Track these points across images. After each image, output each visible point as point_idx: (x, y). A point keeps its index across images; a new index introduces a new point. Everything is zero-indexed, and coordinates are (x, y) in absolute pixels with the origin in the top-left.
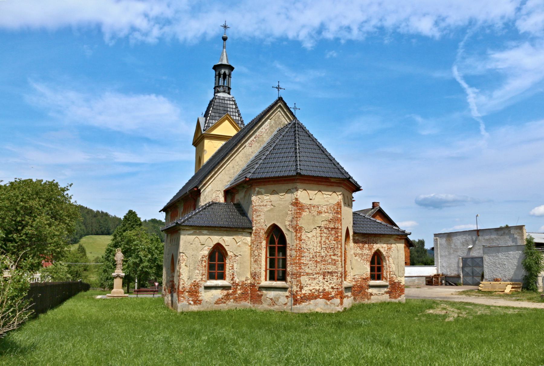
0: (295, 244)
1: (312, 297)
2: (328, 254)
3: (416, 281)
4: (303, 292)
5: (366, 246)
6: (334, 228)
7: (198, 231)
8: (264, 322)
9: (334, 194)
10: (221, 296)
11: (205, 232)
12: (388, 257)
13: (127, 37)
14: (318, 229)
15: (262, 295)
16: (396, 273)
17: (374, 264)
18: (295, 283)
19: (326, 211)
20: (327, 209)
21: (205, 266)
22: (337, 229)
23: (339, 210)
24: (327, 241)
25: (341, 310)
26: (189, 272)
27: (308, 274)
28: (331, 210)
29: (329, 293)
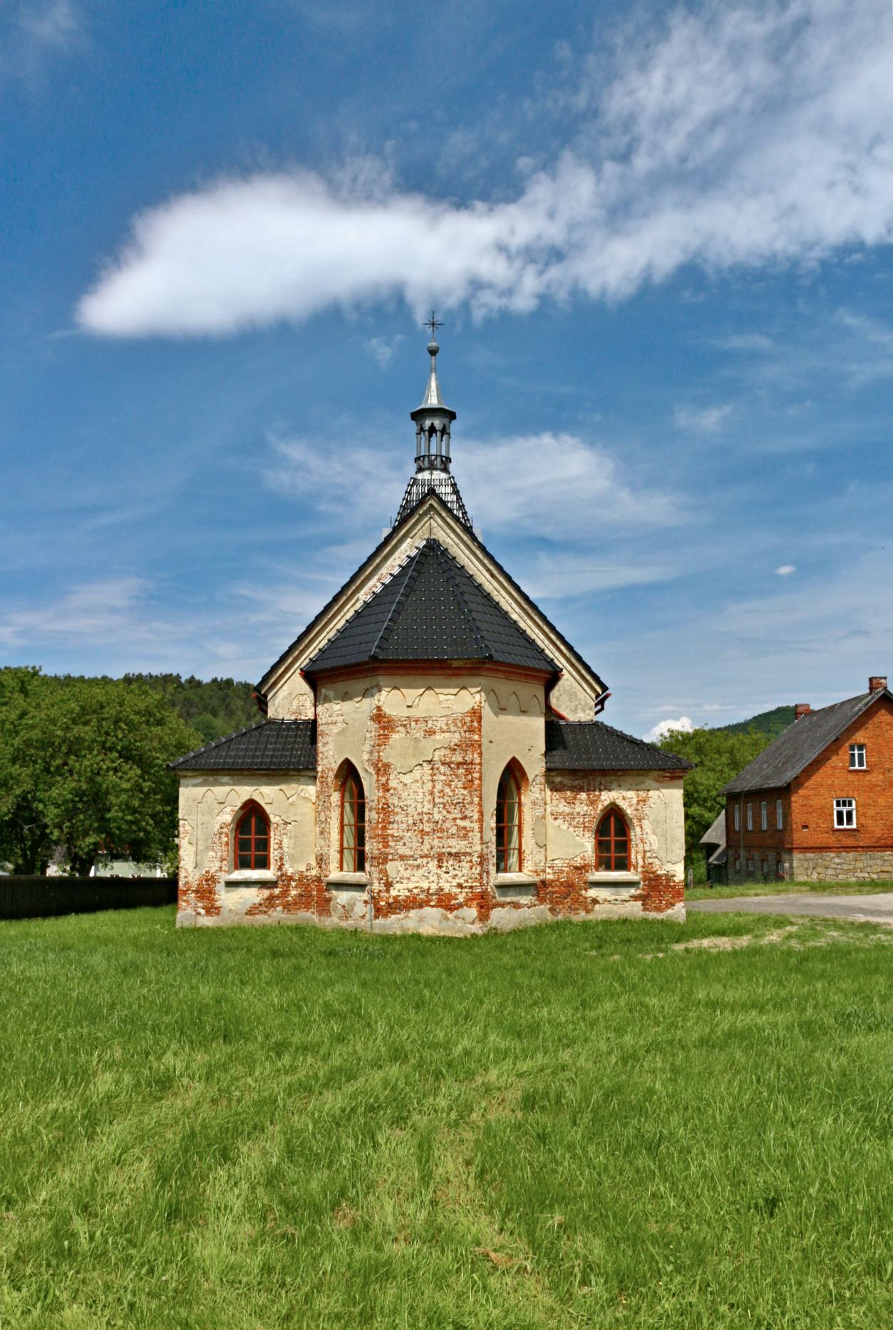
1: (397, 906)
2: (448, 816)
4: (393, 893)
5: (583, 795)
6: (465, 763)
7: (211, 779)
8: (351, 952)
9: (464, 692)
10: (257, 900)
11: (225, 779)
12: (640, 820)
13: (465, 306)
15: (330, 899)
16: (662, 855)
18: (375, 875)
19: (445, 728)
20: (447, 724)
21: (227, 844)
22: (472, 763)
23: (476, 724)
24: (447, 790)
25: (480, 932)
26: (197, 854)
27: (402, 858)
28: (456, 725)
29: (450, 897)
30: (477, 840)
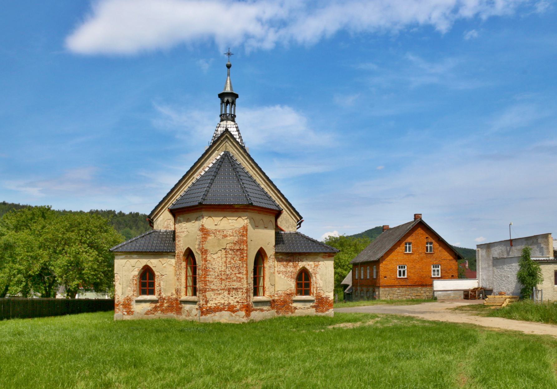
0: (201, 264)
3: (452, 294)
4: (209, 305)
5: (291, 264)
6: (240, 250)
7: (129, 256)
10: (150, 308)
11: (135, 256)
12: (315, 274)
13: (242, 46)
14: (223, 251)
16: (324, 289)
17: (302, 280)
18: (201, 297)
19: (231, 234)
20: (232, 233)
21: (136, 284)
23: (245, 233)
24: (232, 261)
25: (246, 322)
26: (123, 289)
27: (213, 290)
28: (236, 233)
29: (234, 307)
30: (245, 282)
